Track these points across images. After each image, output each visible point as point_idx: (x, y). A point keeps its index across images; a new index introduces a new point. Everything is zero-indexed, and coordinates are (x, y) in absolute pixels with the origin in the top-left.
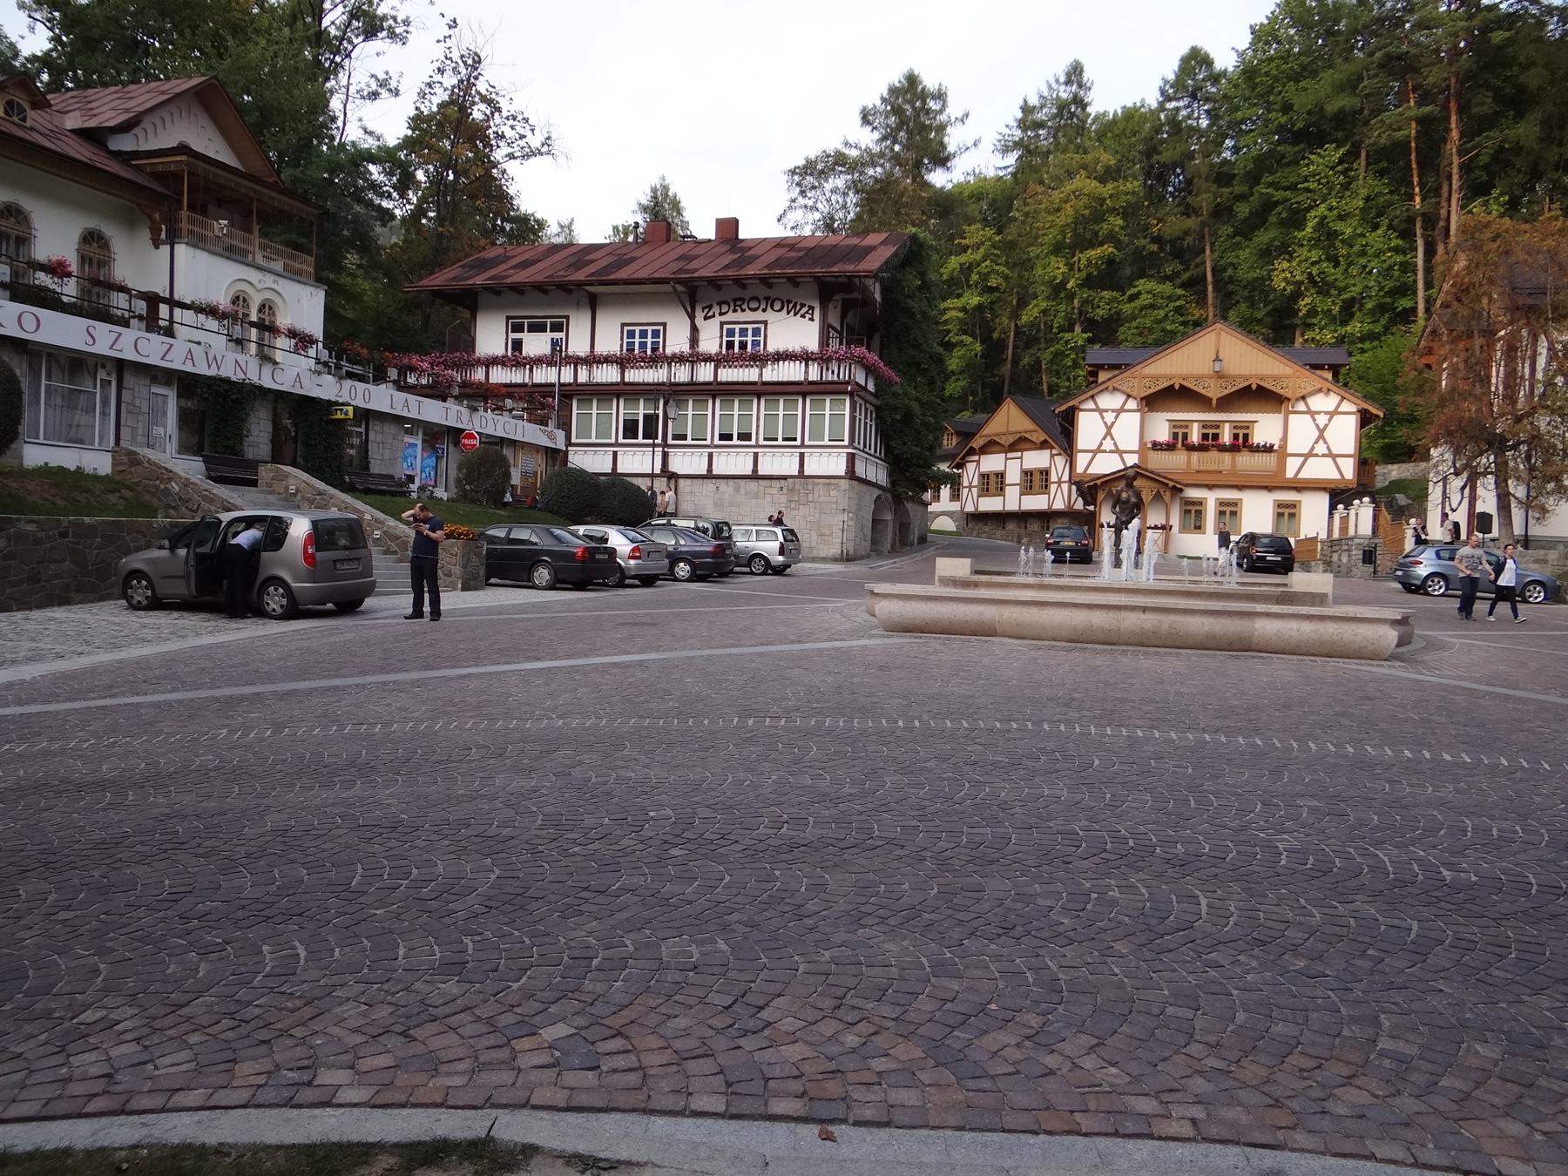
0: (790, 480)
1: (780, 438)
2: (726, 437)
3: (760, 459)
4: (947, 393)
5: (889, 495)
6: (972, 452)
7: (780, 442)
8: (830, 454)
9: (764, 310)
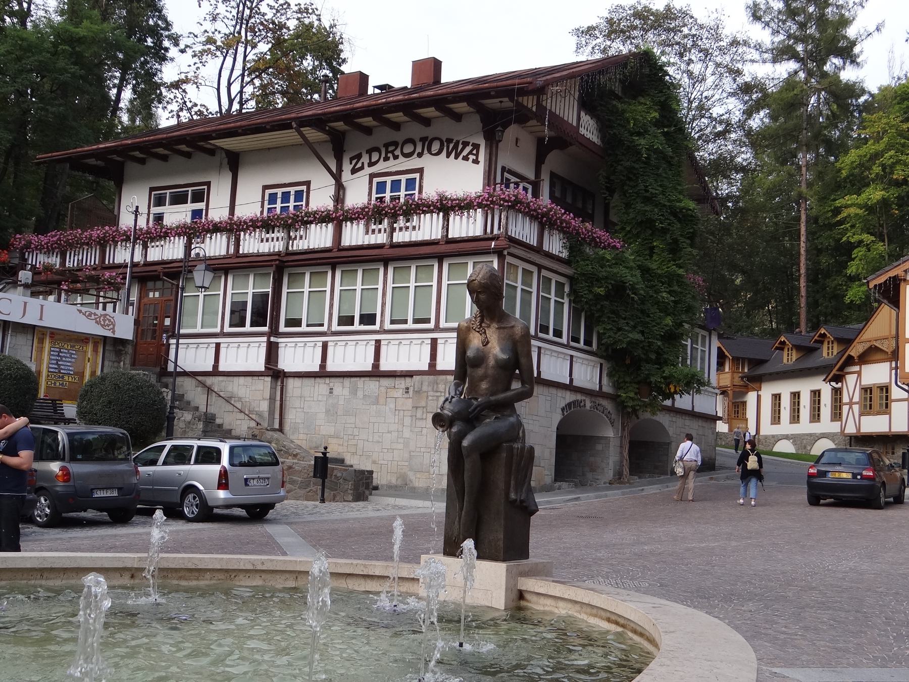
0: (416, 378)
1: (410, 320)
2: (347, 320)
3: (383, 349)
4: (847, 300)
5: (607, 404)
6: (850, 361)
7: (410, 325)
8: (305, 343)
9: (420, 155)
